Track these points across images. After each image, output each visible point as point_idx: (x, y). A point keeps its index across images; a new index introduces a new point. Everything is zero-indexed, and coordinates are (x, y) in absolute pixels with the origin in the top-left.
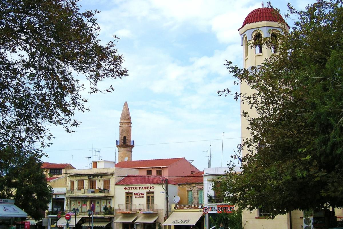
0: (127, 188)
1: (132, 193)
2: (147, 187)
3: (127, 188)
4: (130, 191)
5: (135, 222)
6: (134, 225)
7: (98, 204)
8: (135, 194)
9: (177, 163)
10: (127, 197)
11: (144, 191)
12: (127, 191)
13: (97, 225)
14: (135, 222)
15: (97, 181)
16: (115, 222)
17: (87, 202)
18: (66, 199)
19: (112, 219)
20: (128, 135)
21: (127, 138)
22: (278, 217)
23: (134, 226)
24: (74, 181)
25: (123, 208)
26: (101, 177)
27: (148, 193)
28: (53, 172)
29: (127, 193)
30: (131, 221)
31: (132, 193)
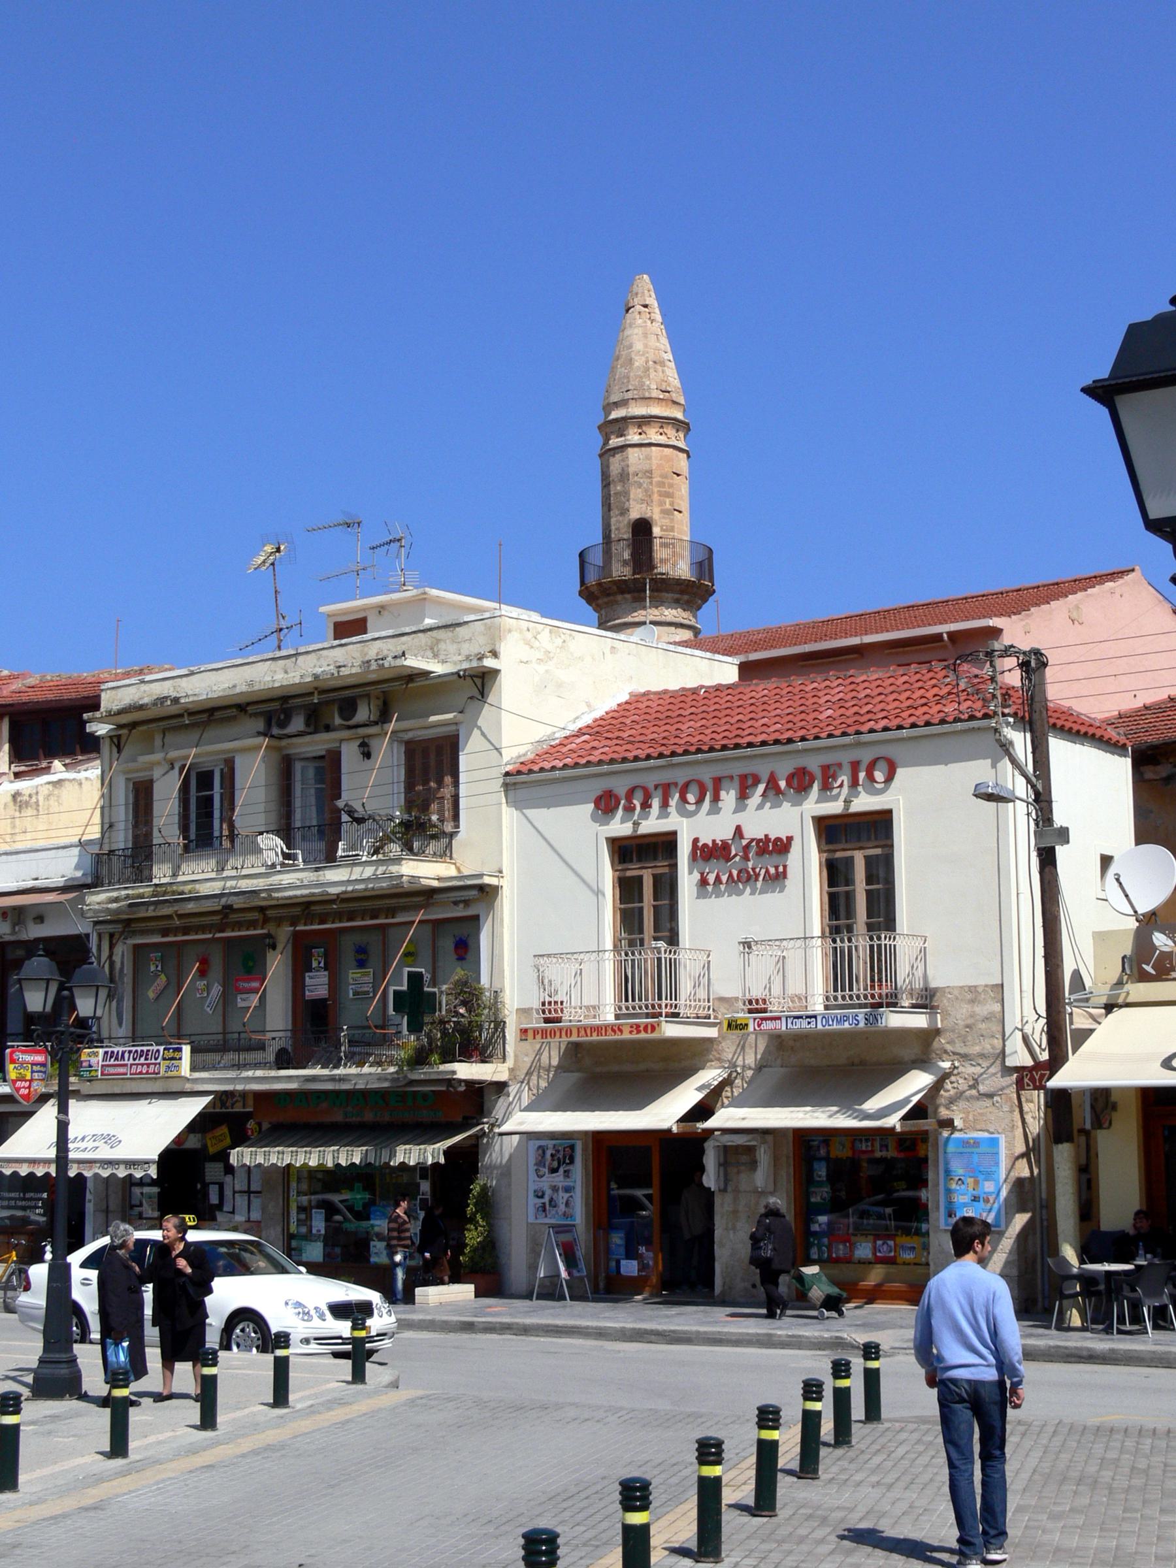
0: (621, 791)
1: (666, 844)
2: (818, 773)
3: (621, 791)
4: (652, 824)
5: (711, 1123)
6: (702, 1152)
7: (361, 964)
8: (705, 853)
9: (1077, 607)
10: (628, 889)
11: (794, 820)
12: (620, 827)
13: (322, 1155)
14: (711, 1123)
15: (349, 753)
16: (505, 1128)
17: (270, 955)
18: (100, 936)
19: (489, 1097)
20: (665, 512)
21: (656, 531)
22: (75, 1352)
23: (702, 1169)
24: (157, 773)
25: (595, 997)
26: (384, 716)
27: (831, 830)
28: (1118, 1445)
29: (624, 851)
30: (665, 1113)
31: (666, 844)
